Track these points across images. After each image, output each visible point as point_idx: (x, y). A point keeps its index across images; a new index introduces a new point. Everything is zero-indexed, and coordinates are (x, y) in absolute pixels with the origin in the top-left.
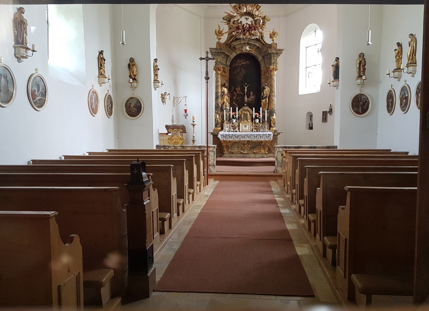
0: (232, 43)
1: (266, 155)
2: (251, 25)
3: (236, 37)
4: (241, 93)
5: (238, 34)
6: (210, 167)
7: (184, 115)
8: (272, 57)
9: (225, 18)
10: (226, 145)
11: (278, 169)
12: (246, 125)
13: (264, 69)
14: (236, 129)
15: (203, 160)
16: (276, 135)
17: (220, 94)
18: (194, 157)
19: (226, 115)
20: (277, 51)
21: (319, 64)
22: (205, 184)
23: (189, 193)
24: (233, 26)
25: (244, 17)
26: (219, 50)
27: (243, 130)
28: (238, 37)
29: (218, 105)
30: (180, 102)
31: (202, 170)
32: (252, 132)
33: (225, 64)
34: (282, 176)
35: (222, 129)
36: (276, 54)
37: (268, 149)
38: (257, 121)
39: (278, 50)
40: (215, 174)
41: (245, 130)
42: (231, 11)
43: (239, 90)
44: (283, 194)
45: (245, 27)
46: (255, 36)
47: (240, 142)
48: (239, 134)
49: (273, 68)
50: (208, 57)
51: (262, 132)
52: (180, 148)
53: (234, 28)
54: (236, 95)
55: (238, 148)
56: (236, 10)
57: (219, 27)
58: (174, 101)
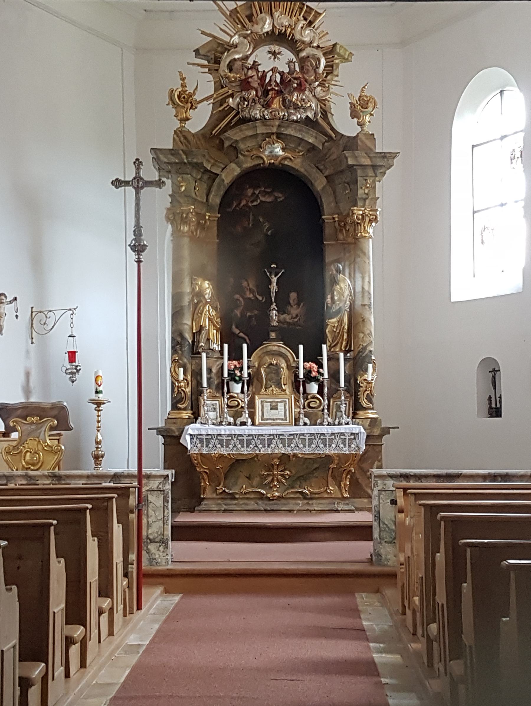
0: (228, 134)
1: (343, 502)
2: (289, 73)
3: (238, 113)
4: (260, 298)
5: (247, 105)
6: (152, 547)
7: (67, 369)
8: (359, 178)
9: (202, 52)
10: (207, 471)
11: (382, 551)
12: (274, 404)
13: (334, 218)
14: (244, 414)
15: (123, 520)
16: (379, 435)
17: (186, 300)
18: (88, 511)
19: (209, 371)
20: (374, 159)
21: (516, 202)
22: (131, 608)
23: (69, 641)
24: (228, 78)
25: (267, 48)
26: (184, 157)
27: (267, 419)
28: (246, 114)
29: (181, 335)
30: (53, 327)
31: (118, 557)
32: (296, 425)
33: (205, 201)
34: (393, 576)
35: (196, 416)
36: (372, 170)
37: (350, 482)
38: (313, 388)
39: (379, 155)
40: (167, 572)
41: (273, 419)
42: (221, 29)
43: (251, 286)
44: (400, 640)
45: (267, 80)
46: (301, 110)
47: (256, 459)
48: (254, 433)
49: (362, 215)
50: (142, 179)
51: (328, 425)
52: (48, 482)
53: (234, 84)
54: (243, 304)
55: (249, 478)
56: (239, 26)
57: (183, 79)
58: (32, 324)
